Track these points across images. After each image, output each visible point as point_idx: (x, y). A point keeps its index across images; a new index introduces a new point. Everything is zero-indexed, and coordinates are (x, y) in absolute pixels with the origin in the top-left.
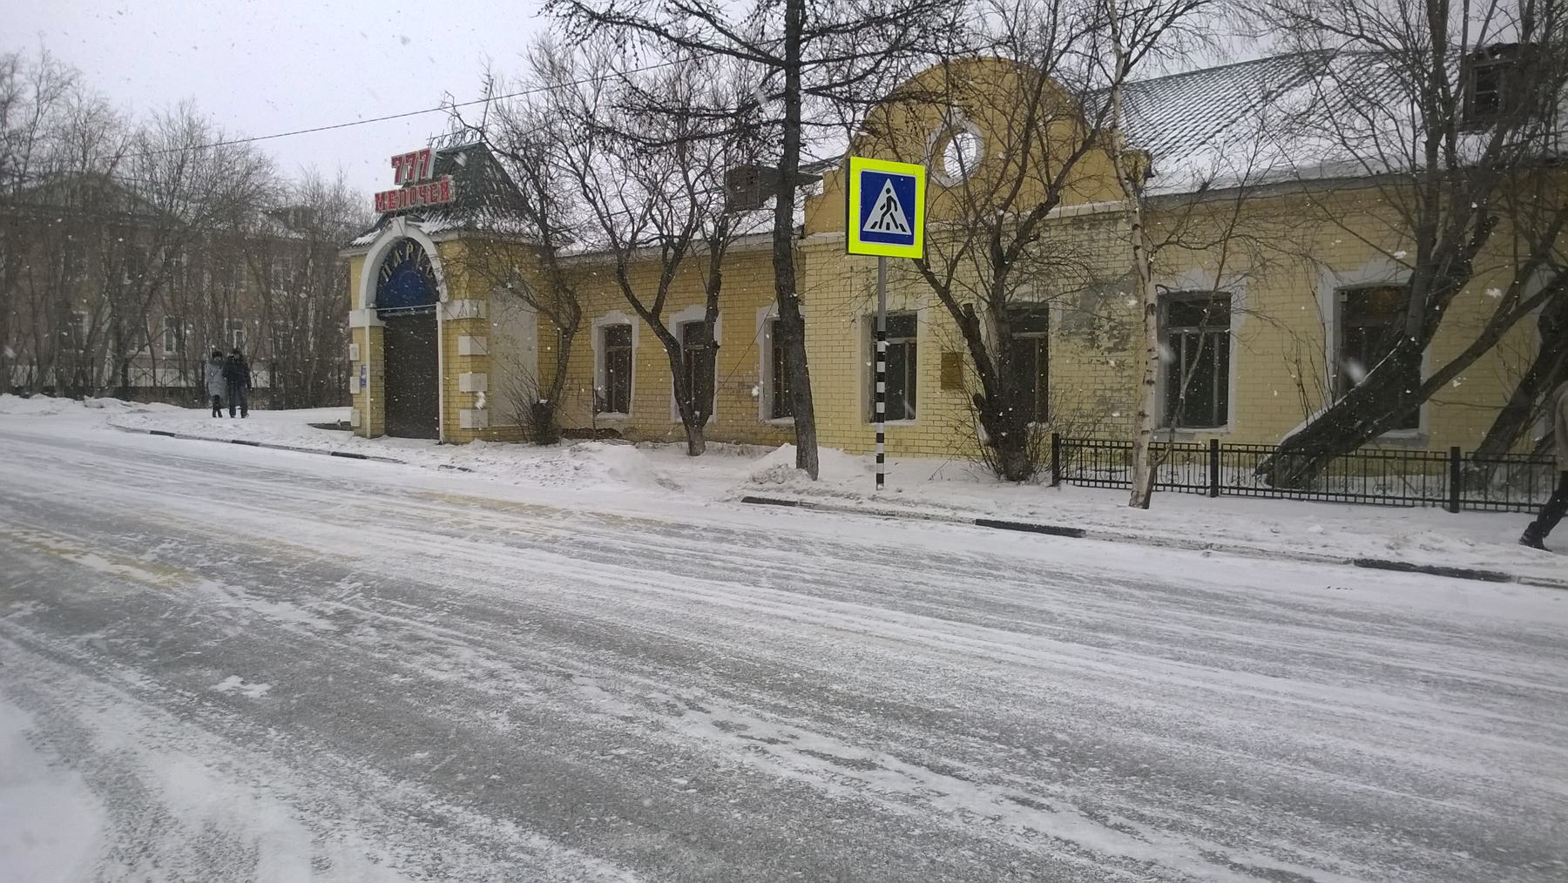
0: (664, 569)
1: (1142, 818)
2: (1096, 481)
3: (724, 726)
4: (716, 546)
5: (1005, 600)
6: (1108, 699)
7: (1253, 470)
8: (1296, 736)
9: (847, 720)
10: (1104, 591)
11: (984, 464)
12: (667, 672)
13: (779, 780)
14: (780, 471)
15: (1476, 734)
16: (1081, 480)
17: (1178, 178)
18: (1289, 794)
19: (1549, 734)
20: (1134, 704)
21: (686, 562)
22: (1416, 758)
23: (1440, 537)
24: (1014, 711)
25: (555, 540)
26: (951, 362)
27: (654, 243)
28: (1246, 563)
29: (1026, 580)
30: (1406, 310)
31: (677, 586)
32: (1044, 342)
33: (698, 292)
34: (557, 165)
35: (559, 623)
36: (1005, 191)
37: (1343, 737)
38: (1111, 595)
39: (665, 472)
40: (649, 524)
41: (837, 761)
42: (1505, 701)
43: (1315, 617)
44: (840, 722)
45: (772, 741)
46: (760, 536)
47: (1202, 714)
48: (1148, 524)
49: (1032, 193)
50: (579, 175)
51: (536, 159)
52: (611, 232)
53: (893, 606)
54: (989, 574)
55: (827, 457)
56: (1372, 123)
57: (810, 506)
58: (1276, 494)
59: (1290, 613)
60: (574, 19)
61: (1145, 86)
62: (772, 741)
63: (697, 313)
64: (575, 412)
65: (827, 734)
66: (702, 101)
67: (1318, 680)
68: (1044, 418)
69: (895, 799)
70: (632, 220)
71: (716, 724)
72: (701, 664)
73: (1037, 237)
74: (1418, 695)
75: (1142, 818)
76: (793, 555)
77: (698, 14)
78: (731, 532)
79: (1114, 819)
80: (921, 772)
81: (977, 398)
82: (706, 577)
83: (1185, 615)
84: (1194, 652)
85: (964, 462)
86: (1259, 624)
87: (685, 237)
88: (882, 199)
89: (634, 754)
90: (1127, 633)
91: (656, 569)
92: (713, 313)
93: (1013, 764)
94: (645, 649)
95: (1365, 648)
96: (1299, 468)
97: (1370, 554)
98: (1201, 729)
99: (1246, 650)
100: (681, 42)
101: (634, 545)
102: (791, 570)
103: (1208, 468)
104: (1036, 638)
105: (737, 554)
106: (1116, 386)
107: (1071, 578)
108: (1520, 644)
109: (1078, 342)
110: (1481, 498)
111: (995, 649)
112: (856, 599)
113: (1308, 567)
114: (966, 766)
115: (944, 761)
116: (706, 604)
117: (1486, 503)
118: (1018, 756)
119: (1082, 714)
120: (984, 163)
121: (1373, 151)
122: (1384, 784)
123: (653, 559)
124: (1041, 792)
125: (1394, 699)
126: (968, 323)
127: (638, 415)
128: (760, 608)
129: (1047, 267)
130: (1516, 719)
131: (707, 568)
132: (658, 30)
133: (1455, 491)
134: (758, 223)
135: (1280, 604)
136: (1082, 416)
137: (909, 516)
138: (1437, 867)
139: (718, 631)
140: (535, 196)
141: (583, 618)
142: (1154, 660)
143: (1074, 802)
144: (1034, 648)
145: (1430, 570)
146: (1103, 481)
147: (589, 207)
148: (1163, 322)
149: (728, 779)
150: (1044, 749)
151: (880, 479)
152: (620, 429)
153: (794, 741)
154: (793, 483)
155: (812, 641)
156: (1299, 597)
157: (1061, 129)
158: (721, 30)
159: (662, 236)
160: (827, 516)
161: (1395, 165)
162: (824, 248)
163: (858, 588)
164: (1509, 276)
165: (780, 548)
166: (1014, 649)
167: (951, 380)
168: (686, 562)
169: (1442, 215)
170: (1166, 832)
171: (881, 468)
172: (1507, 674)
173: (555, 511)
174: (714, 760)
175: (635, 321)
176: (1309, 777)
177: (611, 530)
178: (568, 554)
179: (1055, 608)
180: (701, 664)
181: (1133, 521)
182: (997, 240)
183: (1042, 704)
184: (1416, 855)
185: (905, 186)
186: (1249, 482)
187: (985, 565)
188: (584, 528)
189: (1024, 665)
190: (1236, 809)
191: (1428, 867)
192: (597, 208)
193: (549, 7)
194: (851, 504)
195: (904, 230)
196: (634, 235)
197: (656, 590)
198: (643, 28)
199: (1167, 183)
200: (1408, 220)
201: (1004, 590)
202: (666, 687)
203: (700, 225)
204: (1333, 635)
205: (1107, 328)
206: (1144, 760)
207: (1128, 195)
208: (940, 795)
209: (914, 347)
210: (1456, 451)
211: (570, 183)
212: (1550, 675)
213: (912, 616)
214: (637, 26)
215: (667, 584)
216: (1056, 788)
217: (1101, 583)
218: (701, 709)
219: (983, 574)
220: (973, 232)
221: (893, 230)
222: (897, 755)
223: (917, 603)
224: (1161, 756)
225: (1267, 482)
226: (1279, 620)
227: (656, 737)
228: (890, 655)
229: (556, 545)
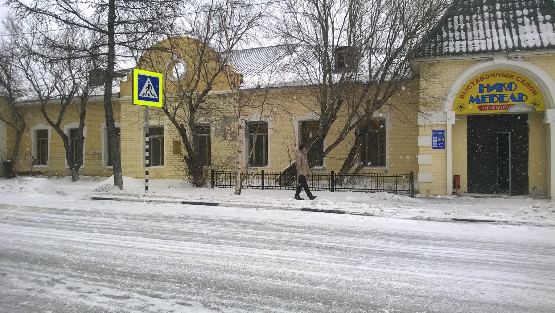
0: (54, 228)
1: (222, 304)
2: (226, 186)
3: (71, 289)
4: (77, 217)
5: (188, 230)
6: (218, 263)
7: (274, 180)
8: (275, 269)
9: (121, 281)
10: (223, 225)
11: (188, 181)
12: (50, 269)
13: (90, 307)
14: (107, 187)
15: (329, 264)
16: (221, 185)
17: (248, 84)
18: (271, 290)
19: (348, 261)
20: (226, 263)
21: (64, 225)
22: (311, 273)
23: (326, 200)
24: (184, 271)
25: (7, 218)
26: (177, 144)
27: (58, 97)
28: (269, 211)
29: (197, 223)
30: (318, 128)
31: (58, 235)
32: (209, 138)
33: (77, 117)
34: (15, 66)
35: (4, 253)
36: (193, 85)
37: (290, 268)
38: (225, 226)
39: (60, 188)
40: (51, 210)
41: (114, 297)
42: (338, 252)
43: (288, 228)
44: (119, 282)
45: (90, 293)
46: (96, 213)
47: (247, 265)
48: (239, 200)
49: (202, 86)
50: (24, 69)
51: (6, 63)
52: (39, 93)
53: (146, 236)
54: (184, 222)
55: (126, 180)
56: (307, 69)
57: (119, 200)
58: (282, 188)
59: (280, 228)
60: (20, 9)
61: (237, 52)
62: (90, 293)
63: (76, 125)
64: (22, 164)
65: (112, 288)
66: (77, 44)
67: (285, 250)
68: (209, 164)
69: (135, 309)
70: (48, 88)
71: (68, 288)
72: (64, 265)
73: (204, 101)
74: (314, 252)
75: (222, 304)
76: (109, 219)
77: (72, 12)
78: (85, 212)
79: (213, 306)
80: (147, 298)
81: (185, 157)
82: (72, 230)
83: (247, 231)
84: (248, 243)
85: (182, 181)
86: (270, 232)
87: (71, 96)
88: (146, 85)
89: (30, 303)
90: (228, 239)
91: (50, 228)
92: (82, 125)
93: (181, 290)
94: (41, 261)
95: (301, 238)
96: (289, 179)
97: (305, 207)
98: (246, 270)
99: (265, 241)
100: (67, 22)
101: (42, 219)
102: (107, 225)
103: (261, 180)
104: (196, 243)
105: (86, 220)
106: (233, 153)
107: (213, 221)
108: (345, 233)
109: (220, 137)
110: (340, 187)
111: (181, 249)
112: (132, 235)
113: (288, 212)
114: (164, 293)
115: (156, 292)
116: (69, 241)
117: (341, 189)
118: (184, 288)
119: (208, 269)
120: (186, 74)
121: (308, 78)
122: (301, 283)
123: (50, 224)
124: (190, 300)
125: (307, 254)
126: (182, 130)
127: (52, 166)
128: (92, 241)
129: (208, 112)
130: (340, 258)
131: (72, 227)
132: (56, 17)
133: (333, 185)
134: (99, 91)
135: (277, 225)
136: (222, 163)
137: (157, 201)
138: (312, 309)
139: (74, 251)
140: (5, 77)
141: (15, 250)
142: (234, 247)
143: (200, 302)
144: (195, 247)
145: (323, 211)
146: (228, 186)
147: (29, 82)
148: (247, 131)
149: (69, 309)
150: (192, 284)
151: (147, 188)
152: (43, 171)
153: (99, 292)
154: (112, 191)
155: (111, 252)
156: (284, 222)
157: (212, 64)
158: (82, 19)
159: (60, 95)
160: (125, 203)
161: (314, 83)
162: (128, 101)
163: (133, 230)
164: (347, 118)
165: (105, 217)
166: (190, 248)
167: (177, 151)
168: (64, 225)
169: (328, 98)
170: (230, 308)
171: (147, 184)
172: (340, 243)
173: (9, 206)
174: (65, 302)
175: (50, 128)
176: (278, 283)
177: (34, 213)
178: (13, 224)
179: (204, 232)
180: (64, 265)
181: (235, 199)
182: (190, 102)
183: (195, 267)
184: (307, 306)
185: (155, 81)
186: (273, 184)
187: (183, 218)
188: (21, 213)
189: (191, 254)
190: (254, 297)
191: (310, 309)
192: (32, 83)
193: (8, 3)
194: (135, 198)
195: (155, 96)
196: (49, 94)
197: (49, 236)
198: (50, 15)
199: (245, 85)
200: (318, 100)
201: (188, 227)
202: (48, 275)
203: (77, 91)
204: (292, 234)
205: (230, 133)
206: (226, 283)
207: (232, 89)
208: (152, 305)
209: (163, 139)
210: (332, 172)
211: (21, 73)
212: (352, 243)
213: (152, 239)
214: (48, 14)
215: (54, 234)
216: (194, 297)
217: (222, 222)
218: (62, 283)
219: (182, 222)
220: (182, 99)
221: (151, 96)
222: (138, 292)
223: (155, 234)
224: (232, 281)
225: (279, 184)
226: (276, 230)
227: (41, 296)
228: (142, 255)
229: (7, 220)
